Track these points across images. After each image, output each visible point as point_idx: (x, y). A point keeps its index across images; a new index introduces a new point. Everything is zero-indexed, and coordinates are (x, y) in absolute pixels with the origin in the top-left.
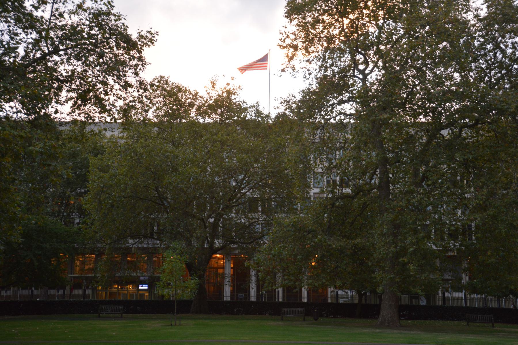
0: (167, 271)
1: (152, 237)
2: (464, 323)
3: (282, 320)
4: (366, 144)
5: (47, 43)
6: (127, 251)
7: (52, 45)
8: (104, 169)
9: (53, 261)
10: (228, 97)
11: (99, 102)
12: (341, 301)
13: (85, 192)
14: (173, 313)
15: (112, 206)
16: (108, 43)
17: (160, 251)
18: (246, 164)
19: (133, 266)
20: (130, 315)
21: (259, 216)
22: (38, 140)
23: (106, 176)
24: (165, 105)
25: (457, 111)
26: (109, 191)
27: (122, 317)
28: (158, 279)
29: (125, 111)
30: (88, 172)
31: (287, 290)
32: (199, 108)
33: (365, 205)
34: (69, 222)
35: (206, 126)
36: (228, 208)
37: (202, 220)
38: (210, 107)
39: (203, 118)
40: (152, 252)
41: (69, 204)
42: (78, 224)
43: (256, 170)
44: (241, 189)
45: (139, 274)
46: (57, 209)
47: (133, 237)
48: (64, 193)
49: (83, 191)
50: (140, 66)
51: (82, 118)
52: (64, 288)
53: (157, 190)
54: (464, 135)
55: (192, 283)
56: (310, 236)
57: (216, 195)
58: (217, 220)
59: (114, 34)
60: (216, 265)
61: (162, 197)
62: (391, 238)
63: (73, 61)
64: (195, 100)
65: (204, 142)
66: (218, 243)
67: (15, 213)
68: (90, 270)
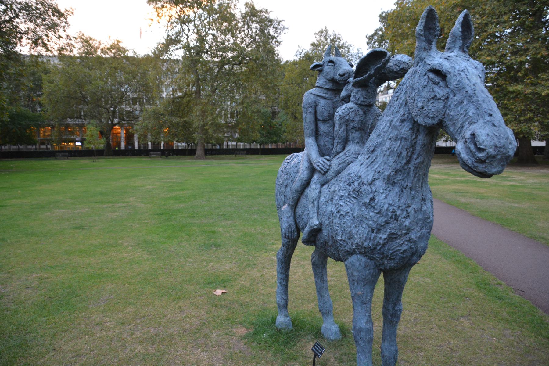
0: (89, 135)
1: (80, 118)
2: (234, 156)
3: (150, 157)
4: (188, 71)
5: (11, 12)
6: (68, 126)
7: (14, 13)
8: (51, 82)
9: (28, 131)
10: (118, 44)
11: (45, 46)
12: (180, 148)
13: (42, 94)
14: (94, 156)
15: (57, 102)
16: (47, 13)
17: (85, 125)
18: (129, 80)
19: (72, 133)
20: (72, 158)
21: (137, 106)
22: (12, 66)
23: (52, 85)
24: (83, 46)
25: (232, 57)
26: (54, 94)
27: (68, 159)
28: (85, 139)
29: (61, 49)
30: (42, 83)
31: (153, 144)
32: (102, 49)
33: (189, 101)
34: (34, 110)
35: (106, 59)
36: (121, 103)
37: (107, 109)
38: (108, 49)
39: (104, 54)
40: (82, 126)
41: (33, 101)
42: (39, 111)
43: (134, 83)
44: (126, 93)
45: (75, 137)
46: (26, 103)
47: (70, 118)
48: (29, 94)
49: (40, 93)
50: (67, 27)
51: (36, 54)
52: (36, 145)
53: (81, 93)
54: (235, 68)
55: (103, 140)
56: (162, 116)
57: (113, 96)
58: (115, 108)
59: (50, 8)
60: (116, 132)
61: (84, 97)
62: (201, 117)
63: (29, 23)
64: (100, 44)
65: (105, 68)
66: (116, 121)
67: (3, 106)
68: (49, 136)
